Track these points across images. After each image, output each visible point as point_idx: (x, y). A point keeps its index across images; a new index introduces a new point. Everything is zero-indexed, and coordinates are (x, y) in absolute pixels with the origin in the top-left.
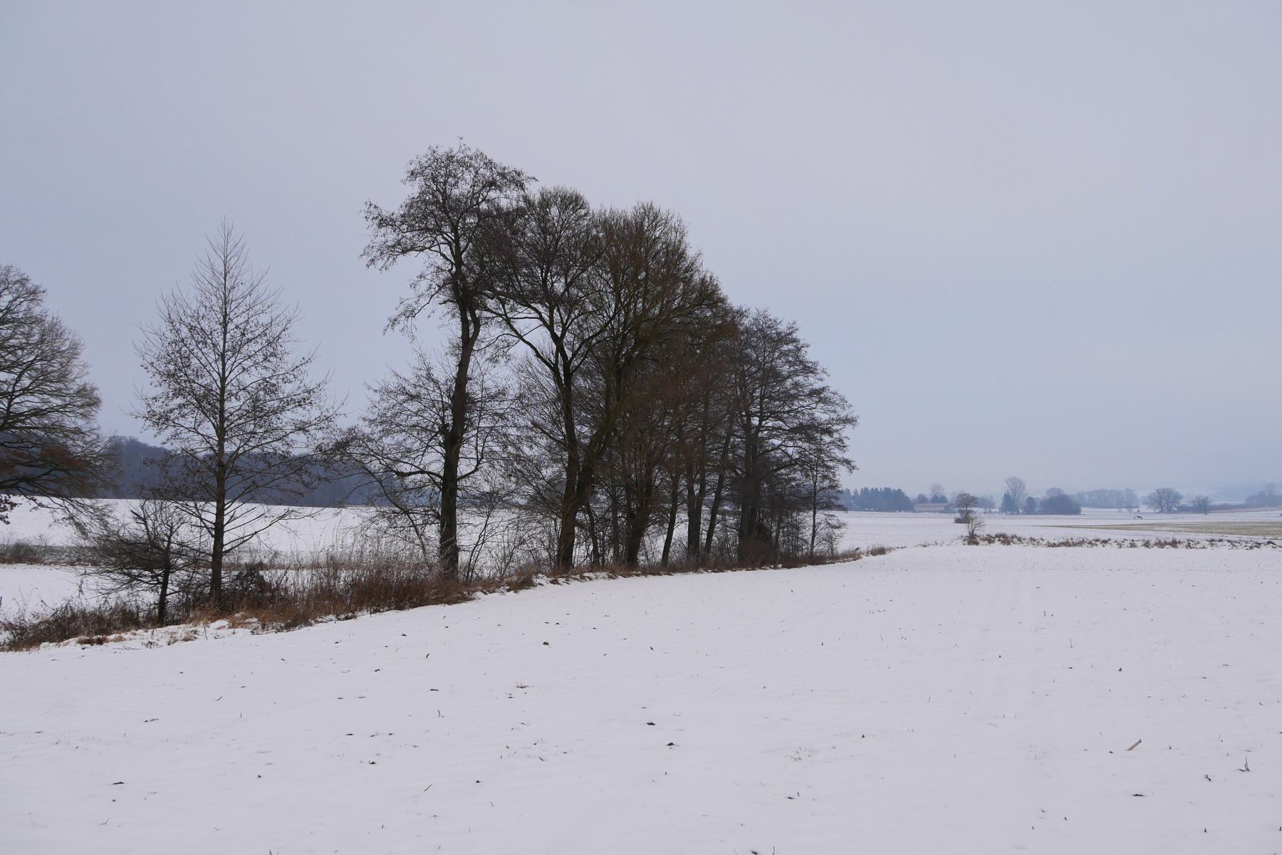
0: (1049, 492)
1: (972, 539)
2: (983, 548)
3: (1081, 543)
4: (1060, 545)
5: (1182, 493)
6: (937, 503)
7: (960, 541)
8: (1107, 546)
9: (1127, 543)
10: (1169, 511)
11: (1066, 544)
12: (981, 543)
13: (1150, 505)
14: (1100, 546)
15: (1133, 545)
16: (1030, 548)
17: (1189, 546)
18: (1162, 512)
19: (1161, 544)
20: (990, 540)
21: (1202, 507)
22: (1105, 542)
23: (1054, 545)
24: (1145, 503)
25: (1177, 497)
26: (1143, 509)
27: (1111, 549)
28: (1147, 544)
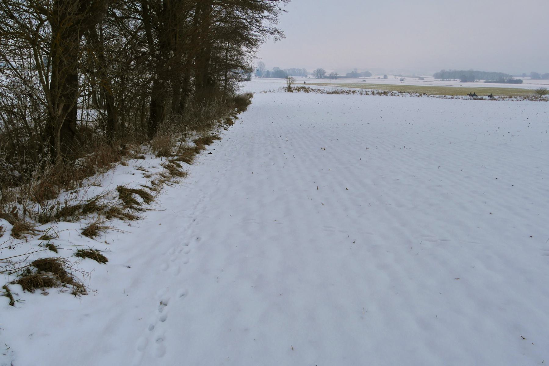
0: (274, 68)
1: (289, 89)
2: (295, 94)
3: (342, 92)
4: (403, 90)
5: (326, 71)
6: (279, 74)
7: (283, 90)
8: (355, 94)
9: (364, 93)
10: (321, 78)
11: (335, 92)
12: (294, 91)
13: (314, 75)
14: (352, 94)
15: (367, 94)
16: (319, 94)
17: (392, 95)
18: (318, 78)
19: (380, 94)
20: (298, 89)
21: (332, 77)
22: (354, 92)
23: (330, 93)
24: (312, 74)
25: (324, 73)
26: (311, 77)
27: (357, 96)
28: (373, 94)
